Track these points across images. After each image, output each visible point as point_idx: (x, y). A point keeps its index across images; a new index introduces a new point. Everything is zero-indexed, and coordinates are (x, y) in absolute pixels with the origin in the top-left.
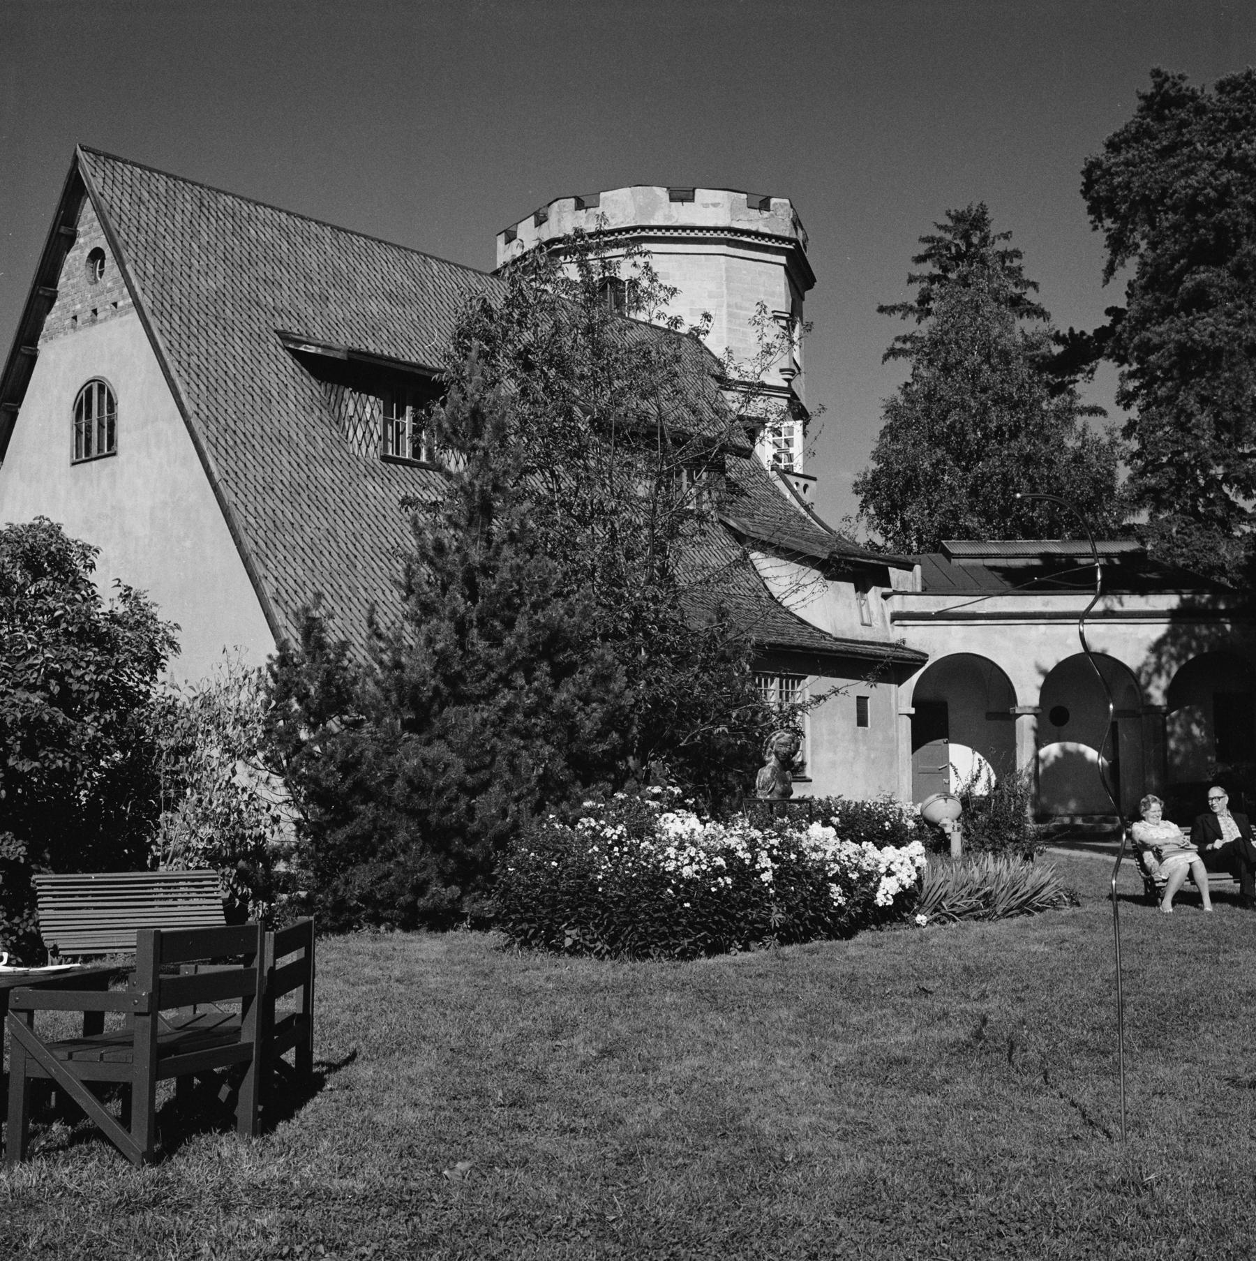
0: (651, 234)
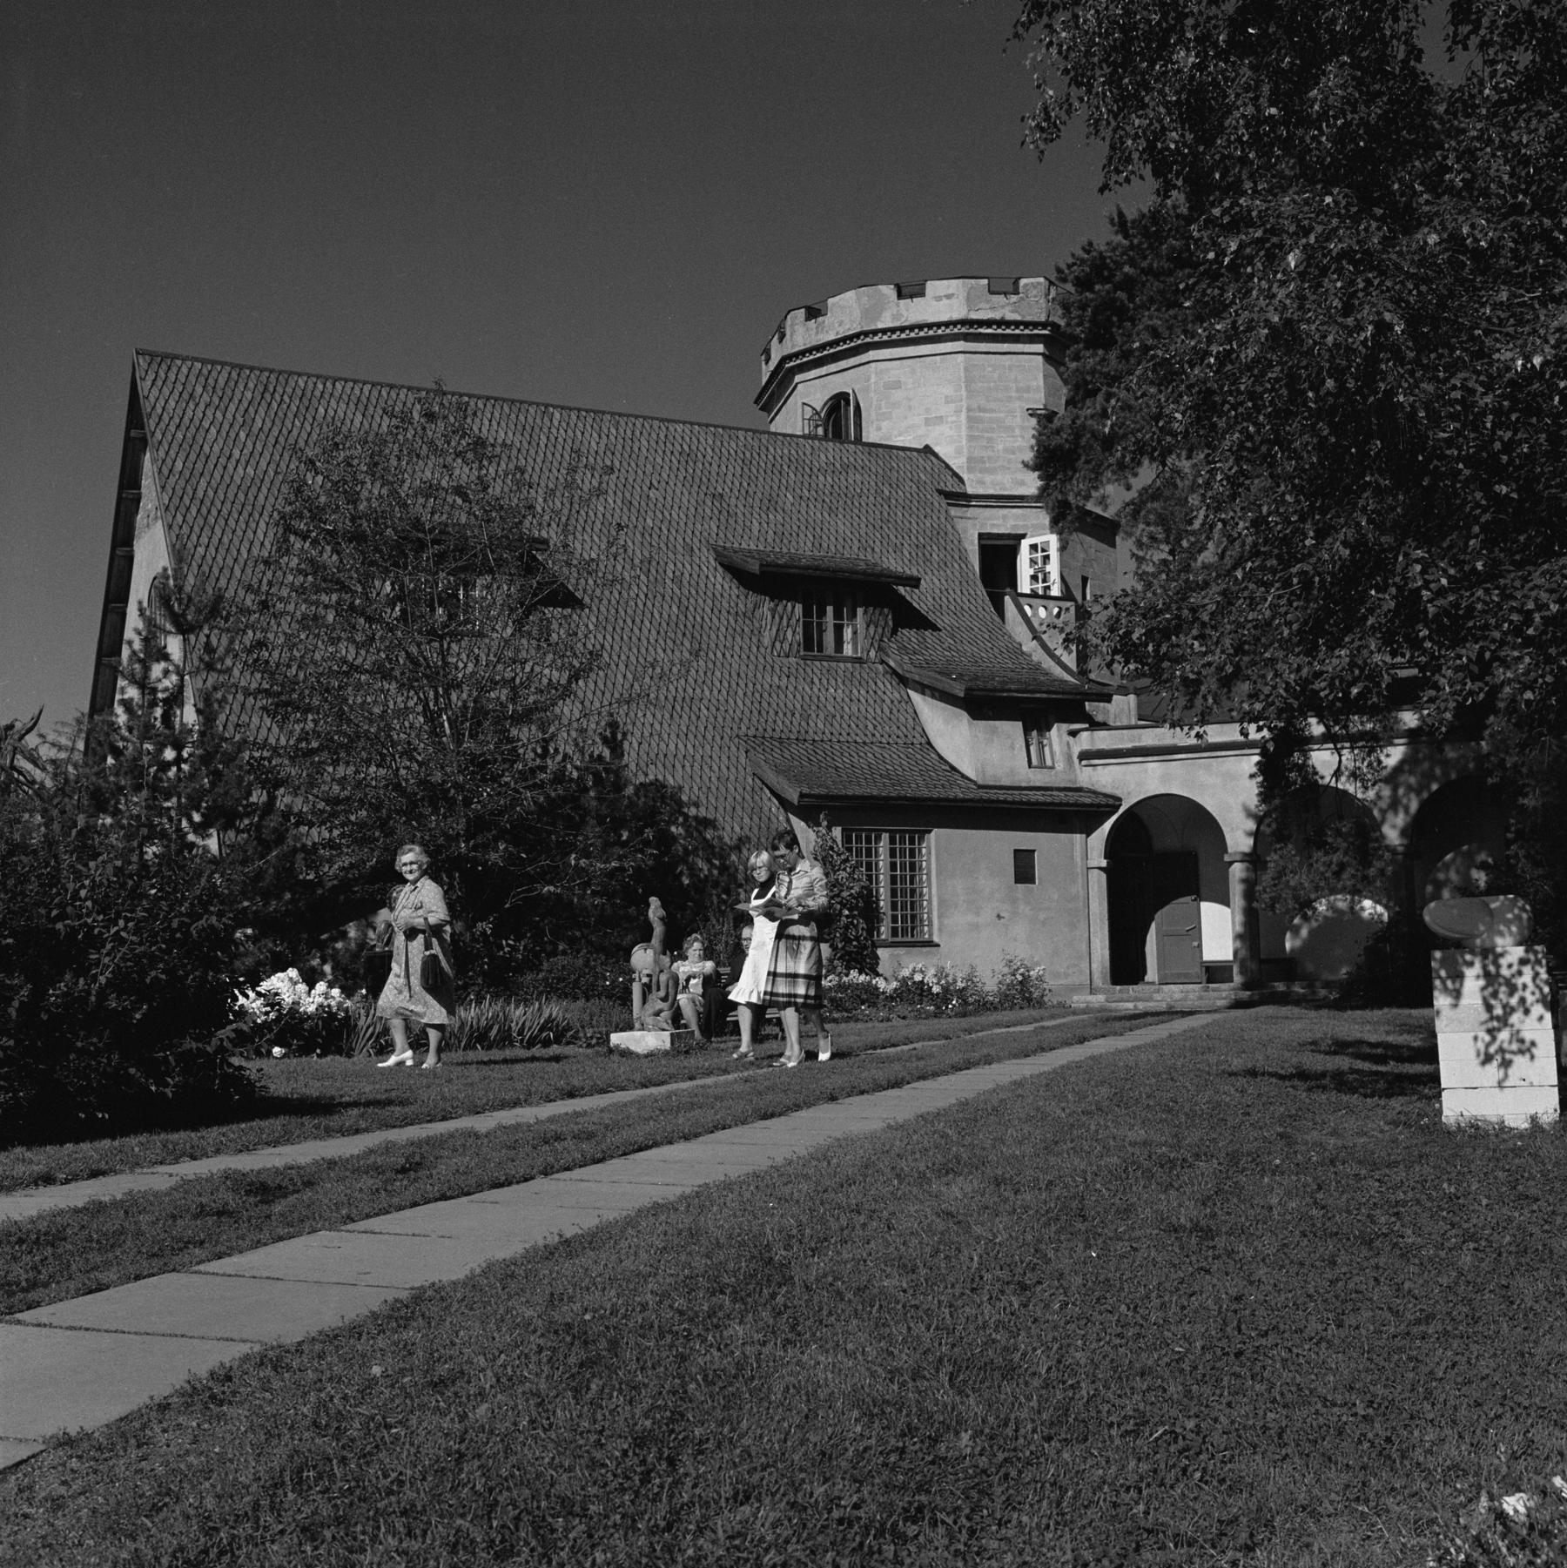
0: (876, 339)
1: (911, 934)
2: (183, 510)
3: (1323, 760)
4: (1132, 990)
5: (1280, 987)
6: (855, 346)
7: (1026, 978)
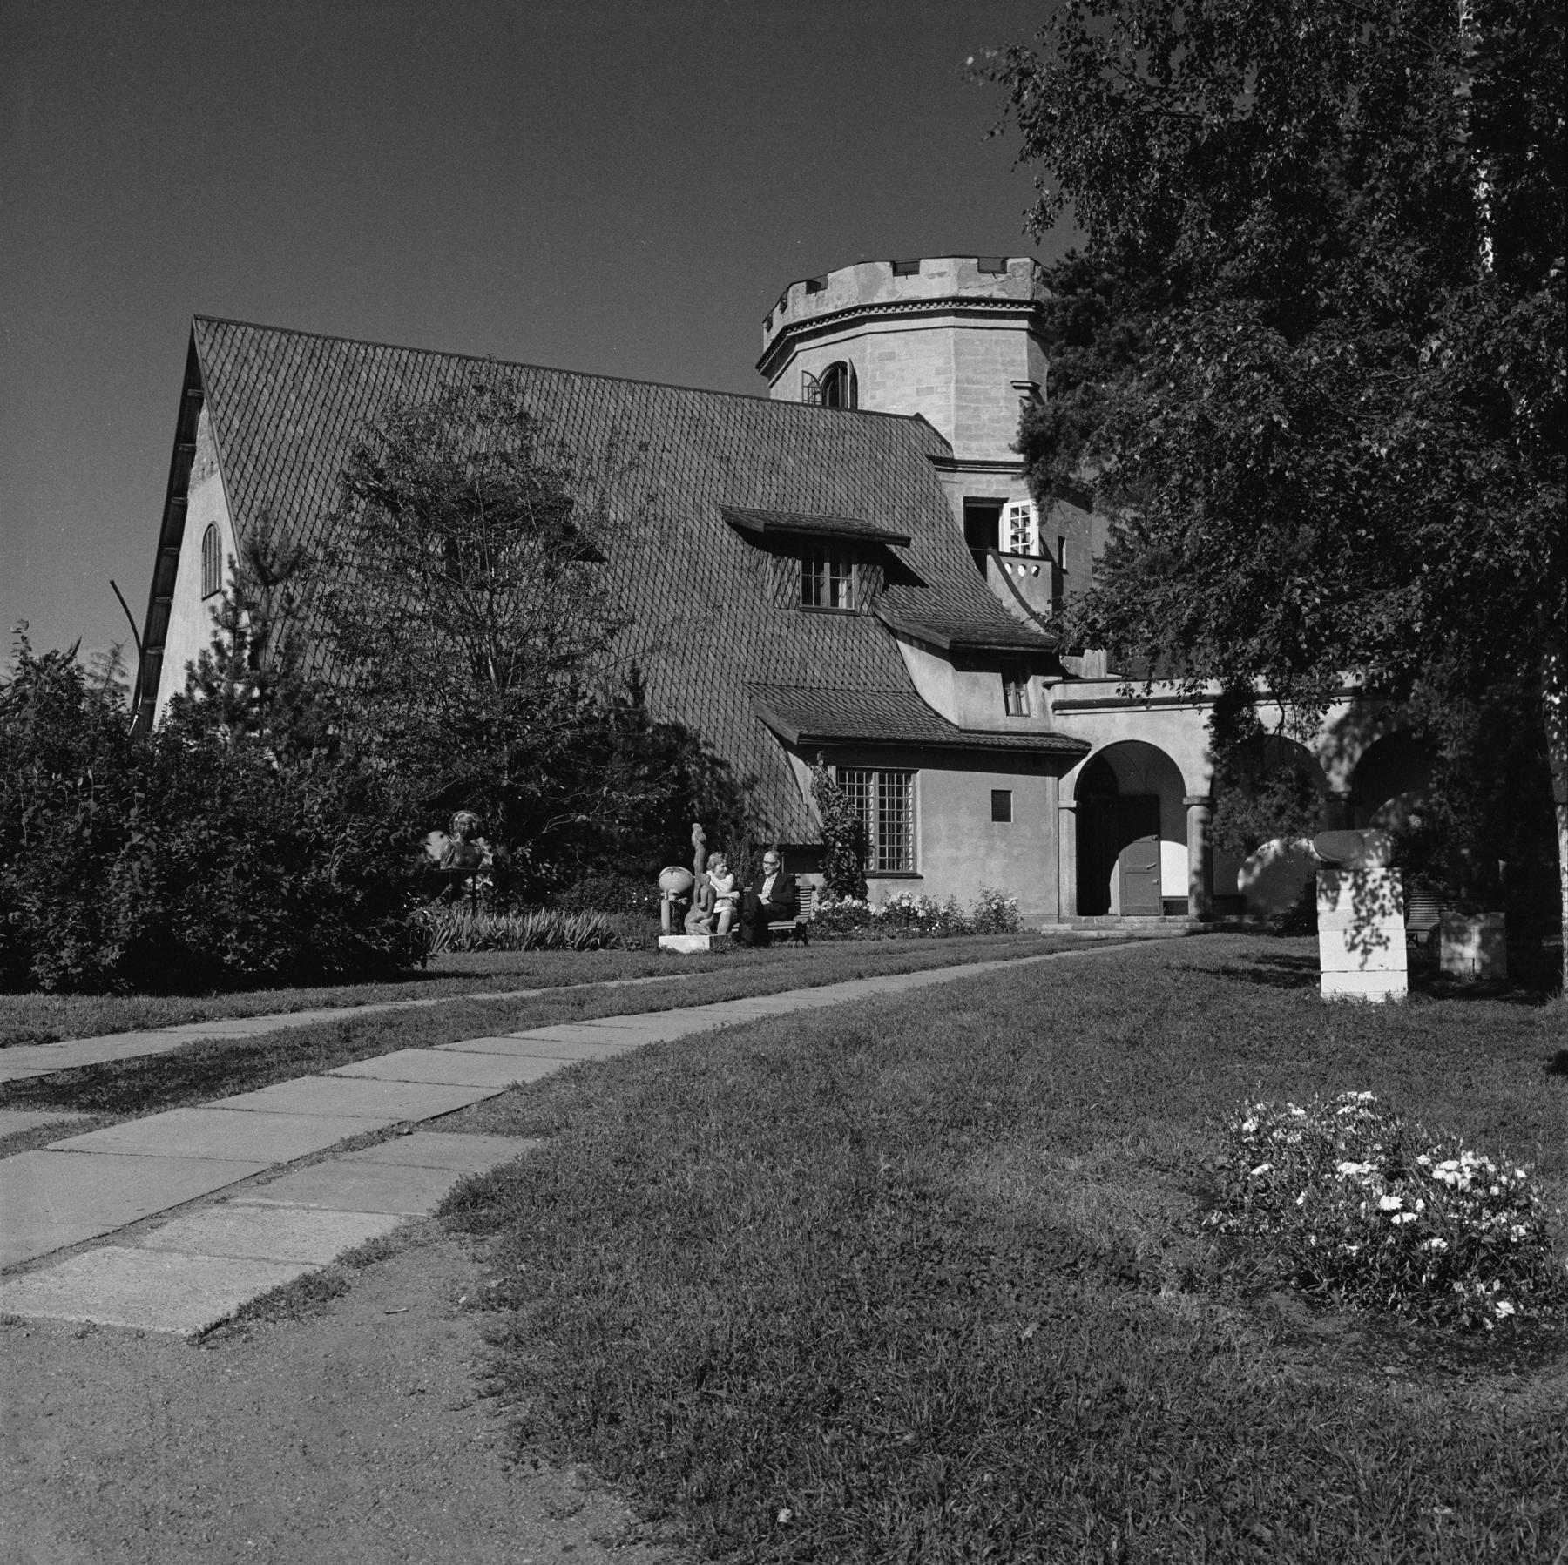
1: (897, 866)
2: (240, 466)
3: (1268, 715)
4: (1096, 920)
5: (1234, 919)
6: (852, 319)
7: (1000, 908)
